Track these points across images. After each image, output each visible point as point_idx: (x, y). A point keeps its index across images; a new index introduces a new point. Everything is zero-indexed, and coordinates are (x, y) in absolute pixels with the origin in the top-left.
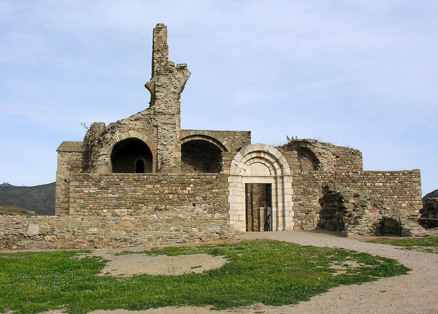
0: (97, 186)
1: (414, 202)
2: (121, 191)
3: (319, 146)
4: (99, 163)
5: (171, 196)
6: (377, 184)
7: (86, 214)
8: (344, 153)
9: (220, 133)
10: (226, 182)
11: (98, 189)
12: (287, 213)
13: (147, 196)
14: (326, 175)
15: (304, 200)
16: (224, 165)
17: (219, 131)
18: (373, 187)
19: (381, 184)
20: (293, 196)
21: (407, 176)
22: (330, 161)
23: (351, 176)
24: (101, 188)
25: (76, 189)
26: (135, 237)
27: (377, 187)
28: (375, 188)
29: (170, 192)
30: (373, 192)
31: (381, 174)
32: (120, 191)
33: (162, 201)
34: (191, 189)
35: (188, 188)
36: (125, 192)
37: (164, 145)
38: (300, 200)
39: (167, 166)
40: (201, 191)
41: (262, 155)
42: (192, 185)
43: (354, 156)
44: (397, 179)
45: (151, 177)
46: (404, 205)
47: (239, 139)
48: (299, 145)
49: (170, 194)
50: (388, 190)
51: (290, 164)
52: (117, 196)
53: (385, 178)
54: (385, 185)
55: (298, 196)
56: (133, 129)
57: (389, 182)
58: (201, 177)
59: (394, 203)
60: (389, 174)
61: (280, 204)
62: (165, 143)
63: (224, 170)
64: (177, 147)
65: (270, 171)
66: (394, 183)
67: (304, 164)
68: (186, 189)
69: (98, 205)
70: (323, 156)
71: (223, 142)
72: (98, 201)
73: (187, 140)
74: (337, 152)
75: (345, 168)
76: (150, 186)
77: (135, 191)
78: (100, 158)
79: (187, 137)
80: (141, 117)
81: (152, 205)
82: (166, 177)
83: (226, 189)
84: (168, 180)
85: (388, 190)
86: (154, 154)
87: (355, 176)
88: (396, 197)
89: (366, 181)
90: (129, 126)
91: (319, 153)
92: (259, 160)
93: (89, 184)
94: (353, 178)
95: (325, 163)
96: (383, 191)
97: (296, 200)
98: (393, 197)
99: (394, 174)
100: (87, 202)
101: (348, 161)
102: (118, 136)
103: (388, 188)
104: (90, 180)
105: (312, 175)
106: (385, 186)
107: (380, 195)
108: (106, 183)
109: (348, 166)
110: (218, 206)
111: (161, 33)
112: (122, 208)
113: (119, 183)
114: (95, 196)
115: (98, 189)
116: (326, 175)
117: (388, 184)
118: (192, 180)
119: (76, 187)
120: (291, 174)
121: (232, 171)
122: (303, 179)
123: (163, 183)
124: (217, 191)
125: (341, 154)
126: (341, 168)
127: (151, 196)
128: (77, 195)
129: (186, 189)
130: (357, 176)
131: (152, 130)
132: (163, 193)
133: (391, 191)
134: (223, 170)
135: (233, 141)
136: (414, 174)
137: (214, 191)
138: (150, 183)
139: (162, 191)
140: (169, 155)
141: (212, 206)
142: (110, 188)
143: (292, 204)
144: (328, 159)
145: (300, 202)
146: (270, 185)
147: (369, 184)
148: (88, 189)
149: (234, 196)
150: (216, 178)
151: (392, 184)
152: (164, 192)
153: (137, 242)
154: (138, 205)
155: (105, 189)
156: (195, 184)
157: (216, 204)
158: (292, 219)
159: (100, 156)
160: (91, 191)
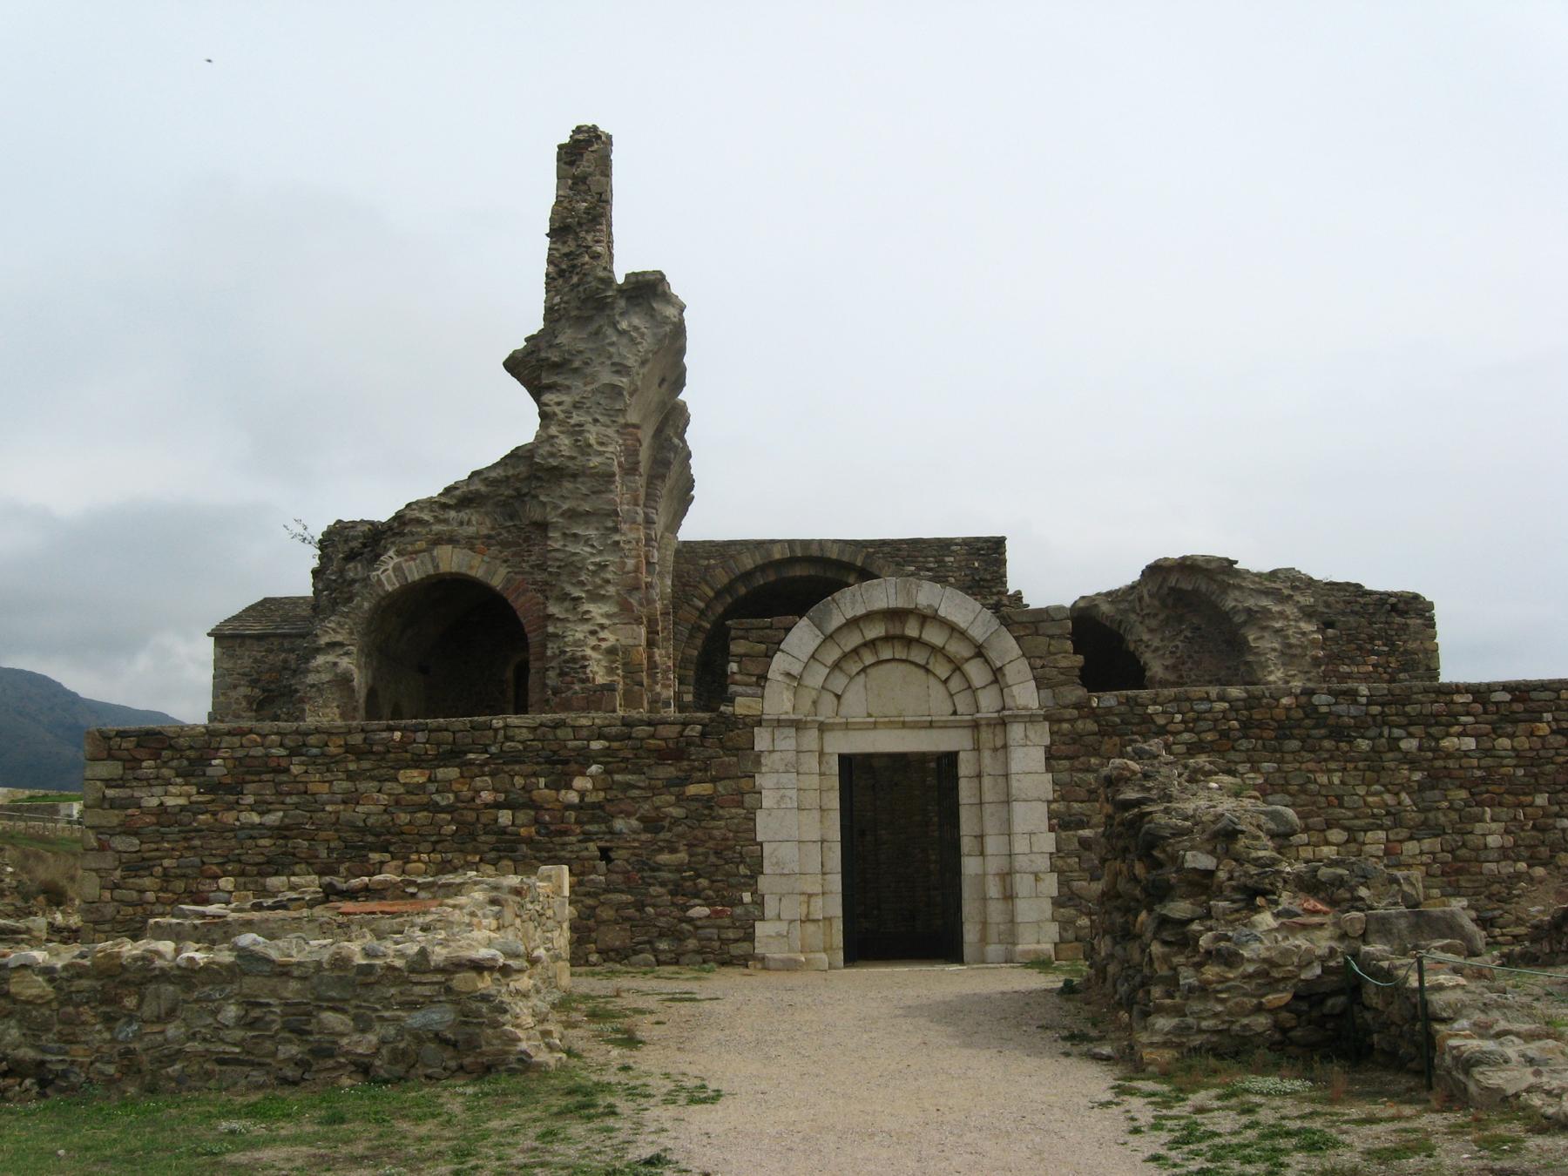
0: (194, 780)
2: (295, 799)
4: (311, 678)
5: (505, 817)
7: (150, 896)
8: (1357, 608)
10: (745, 750)
11: (199, 793)
12: (1023, 884)
13: (404, 818)
14: (1203, 707)
16: (738, 677)
18: (1430, 754)
19: (1470, 743)
20: (1054, 806)
23: (1324, 709)
24: (213, 788)
25: (110, 793)
26: (60, 1052)
27: (1449, 756)
28: (1439, 763)
29: (502, 797)
30: (1435, 779)
31: (1468, 698)
32: (288, 800)
34: (589, 786)
35: (579, 782)
36: (312, 804)
38: (1081, 825)
39: (577, 687)
40: (636, 793)
41: (912, 630)
42: (594, 769)
43: (1398, 620)
44: (1548, 716)
45: (421, 737)
47: (960, 568)
48: (1165, 579)
49: (498, 806)
50: (1503, 770)
51: (1039, 662)
52: (273, 818)
53: (1485, 712)
54: (1489, 745)
55: (1075, 805)
56: (452, 540)
57: (1510, 730)
59: (1534, 827)
60: (1508, 697)
61: (993, 844)
63: (738, 699)
65: (951, 695)
66: (1532, 734)
67: (1190, 657)
68: (569, 787)
69: (197, 860)
72: (197, 842)
73: (760, 581)
74: (1327, 605)
75: (1363, 669)
76: (415, 776)
77: (352, 799)
78: (320, 660)
79: (762, 568)
80: (483, 489)
81: (424, 857)
83: (744, 784)
84: (493, 749)
85: (1503, 770)
86: (533, 638)
87: (1342, 709)
88: (1541, 799)
89: (1397, 732)
92: (900, 653)
93: (165, 772)
94: (1332, 721)
96: (1478, 773)
97: (1065, 826)
98: (1529, 799)
99: (1534, 695)
100: (153, 846)
101: (1371, 639)
102: (390, 572)
103: (1506, 761)
104: (166, 754)
106: (1488, 752)
107: (1463, 794)
108: (230, 763)
110: (713, 859)
111: (586, 165)
112: (297, 869)
113: (284, 763)
114: (186, 820)
115: (199, 793)
116: (1203, 707)
117: (1505, 742)
118: (596, 745)
119: (109, 783)
120: (1041, 707)
121: (778, 701)
122: (1095, 728)
123: (471, 763)
124: (703, 789)
125: (1343, 613)
126: (1344, 669)
130: (1353, 710)
131: (527, 539)
132: (472, 805)
133: (1520, 772)
134: (731, 701)
137: (692, 790)
138: (417, 762)
140: (593, 641)
141: (683, 856)
142: (250, 787)
143: (1048, 842)
146: (951, 759)
147: (1409, 745)
148: (158, 790)
149: (781, 813)
150: (703, 735)
151: (1523, 742)
152: (478, 801)
153: (73, 1079)
155: (230, 789)
157: (700, 850)
158: (1047, 907)
159: (318, 650)
160: (170, 802)
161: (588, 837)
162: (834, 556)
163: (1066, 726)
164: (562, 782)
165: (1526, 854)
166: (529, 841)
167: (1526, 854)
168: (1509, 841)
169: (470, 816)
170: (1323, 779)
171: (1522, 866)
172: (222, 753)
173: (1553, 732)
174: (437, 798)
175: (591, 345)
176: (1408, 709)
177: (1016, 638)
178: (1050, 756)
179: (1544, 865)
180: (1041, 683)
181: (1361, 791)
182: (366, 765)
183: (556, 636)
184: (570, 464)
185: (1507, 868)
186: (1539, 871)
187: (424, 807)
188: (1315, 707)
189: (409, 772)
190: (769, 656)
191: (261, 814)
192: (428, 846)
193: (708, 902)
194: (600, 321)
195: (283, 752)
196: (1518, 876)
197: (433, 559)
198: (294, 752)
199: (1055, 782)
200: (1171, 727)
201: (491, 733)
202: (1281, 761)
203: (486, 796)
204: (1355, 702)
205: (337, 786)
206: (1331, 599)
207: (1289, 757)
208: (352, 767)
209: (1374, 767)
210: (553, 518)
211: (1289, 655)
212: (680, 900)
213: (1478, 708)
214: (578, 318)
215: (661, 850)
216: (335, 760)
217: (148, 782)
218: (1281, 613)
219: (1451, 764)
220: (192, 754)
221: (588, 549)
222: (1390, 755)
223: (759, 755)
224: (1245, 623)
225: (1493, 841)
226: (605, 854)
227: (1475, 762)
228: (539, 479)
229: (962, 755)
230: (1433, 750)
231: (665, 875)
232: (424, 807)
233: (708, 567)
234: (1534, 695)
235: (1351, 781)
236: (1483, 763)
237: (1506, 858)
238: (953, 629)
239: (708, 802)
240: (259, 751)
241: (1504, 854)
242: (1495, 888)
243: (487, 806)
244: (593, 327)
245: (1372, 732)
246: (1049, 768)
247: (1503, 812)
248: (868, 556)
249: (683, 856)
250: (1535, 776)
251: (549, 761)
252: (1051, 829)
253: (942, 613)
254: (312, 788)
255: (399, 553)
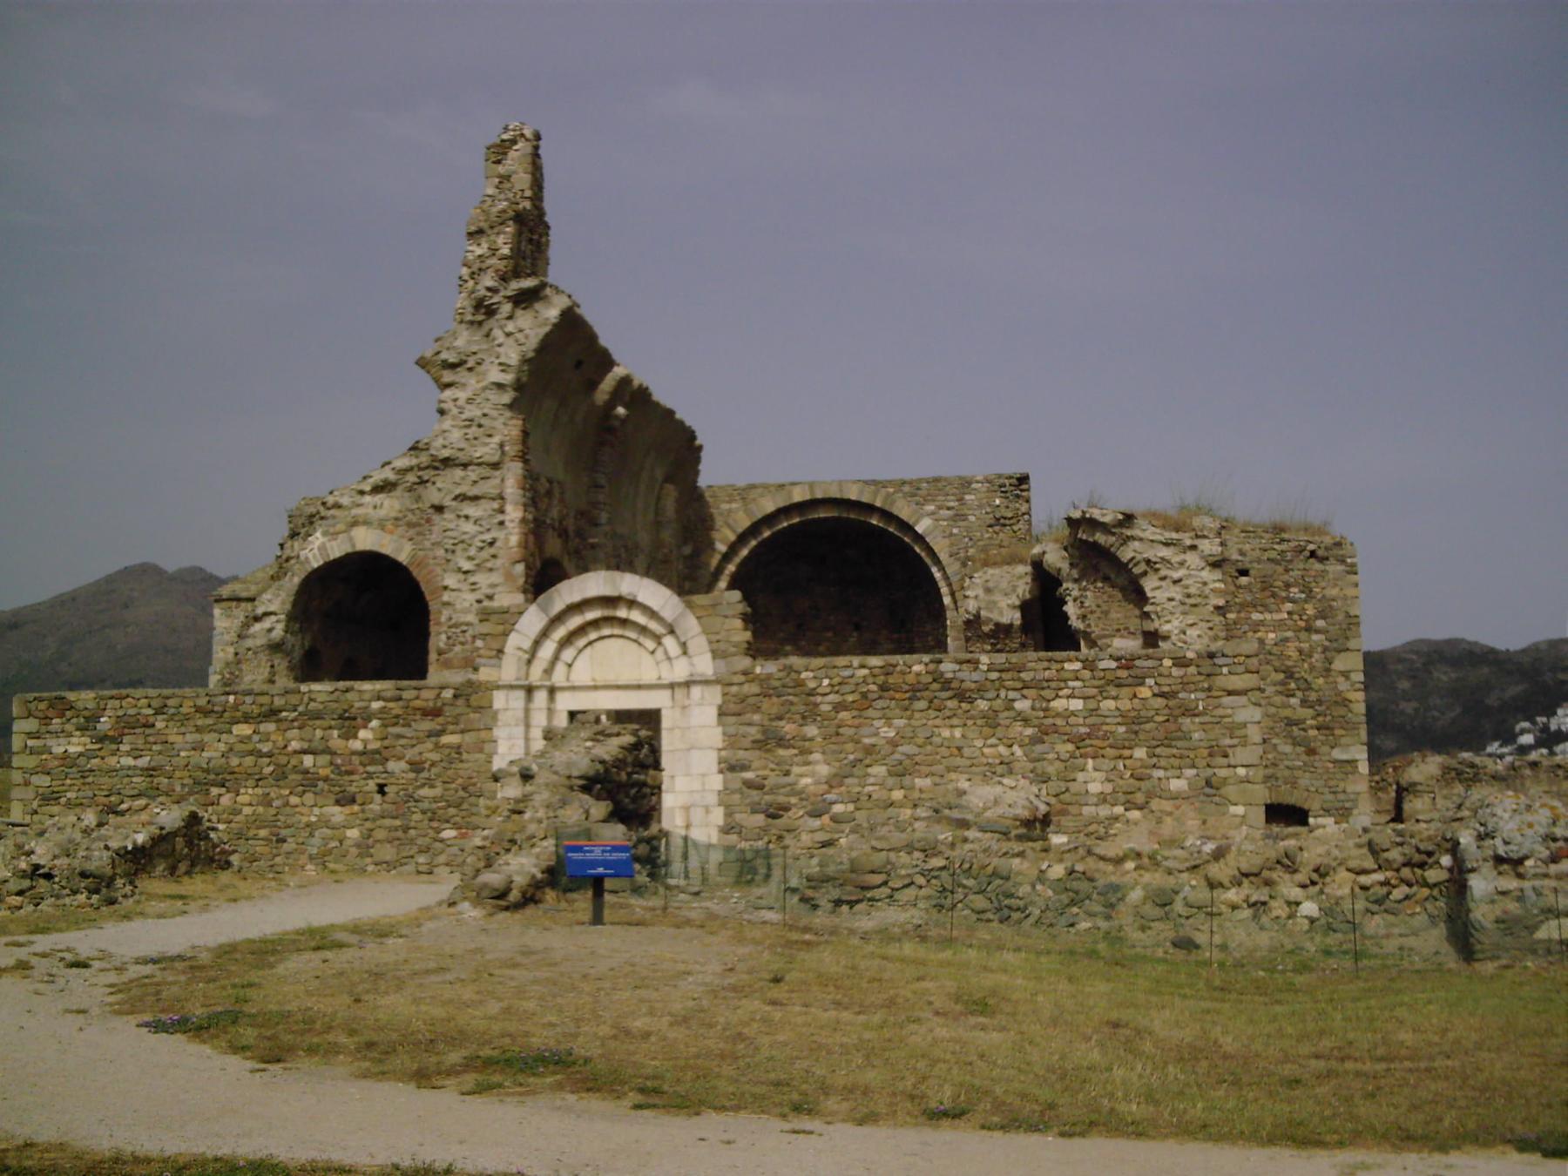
1: (1223, 773)
3: (1147, 535)
5: (308, 761)
6: (1059, 704)
8: (1273, 554)
9: (906, 488)
10: (485, 708)
14: (847, 673)
15: (765, 768)
17: (904, 483)
18: (1041, 714)
19: (1076, 704)
20: (723, 753)
21: (1192, 670)
22: (1192, 590)
23: (950, 675)
24: (102, 739)
25: (30, 743)
27: (1058, 715)
28: (1049, 721)
30: (1044, 733)
32: (154, 747)
33: (280, 776)
37: (466, 572)
38: (744, 768)
40: (403, 742)
41: (622, 613)
42: (375, 723)
43: (1318, 566)
45: (249, 699)
46: (1177, 785)
47: (980, 507)
49: (305, 752)
52: (143, 762)
56: (367, 523)
57: (1113, 693)
58: (406, 695)
60: (1113, 664)
62: (467, 566)
64: (509, 576)
66: (1135, 696)
68: (355, 737)
70: (1163, 573)
71: (917, 522)
72: (90, 780)
74: (1242, 553)
75: (1277, 616)
76: (243, 730)
77: (199, 747)
82: (294, 699)
83: (483, 734)
85: (1105, 728)
88: (1140, 753)
89: (1012, 695)
90: (355, 511)
91: (1148, 562)
92: (617, 631)
93: (69, 727)
94: (955, 685)
95: (1171, 600)
97: (732, 768)
101: (1288, 586)
105: (793, 675)
106: (1094, 711)
107: (1070, 747)
109: (1289, 606)
110: (461, 793)
113: (151, 720)
116: (847, 673)
117: (1111, 704)
118: (376, 705)
119: (31, 735)
125: (1259, 561)
126: (1256, 616)
127: (249, 761)
128: (31, 762)
129: (355, 737)
130: (976, 676)
131: (428, 521)
133: (1122, 729)
135: (959, 517)
136: (1229, 661)
137: (445, 739)
138: (246, 719)
139: (281, 744)
144: (1187, 587)
145: (749, 775)
148: (61, 740)
150: (455, 696)
151: (1125, 704)
154: (207, 792)
156: (389, 720)
160: (72, 749)
161: (370, 776)
162: (853, 498)
163: (734, 689)
164: (350, 734)
165: (1122, 798)
166: (326, 779)
167: (1122, 798)
168: (1108, 788)
169: (283, 760)
170: (946, 733)
171: (1119, 810)
172: (108, 713)
173: (1155, 695)
174: (259, 746)
175: (485, 346)
176: (1023, 675)
177: (698, 618)
178: (722, 713)
179: (1140, 808)
180: (715, 655)
181: (979, 743)
182: (209, 721)
183: (448, 604)
184: (460, 454)
185: (1104, 811)
186: (1135, 814)
187: (251, 753)
188: (942, 674)
189: (241, 726)
190: (506, 634)
191: (135, 758)
192: (251, 783)
193: (457, 827)
194: (492, 323)
195: (151, 712)
196: (1116, 818)
197: (351, 539)
198: (159, 711)
199: (724, 734)
200: (820, 690)
201: (298, 697)
202: (909, 718)
203: (295, 745)
204: (976, 669)
205: (189, 737)
206: (1247, 547)
207: (917, 715)
208: (200, 722)
209: (991, 721)
210: (447, 502)
211: (1190, 604)
212: (435, 824)
213: (1087, 674)
214: (472, 323)
215: (423, 785)
216: (187, 717)
217: (56, 734)
218: (1182, 564)
219: (1059, 722)
220: (86, 713)
221: (477, 528)
222: (1006, 714)
223: (496, 713)
224: (1145, 573)
225: (1094, 788)
226: (381, 789)
227: (1081, 721)
228: (436, 468)
229: (664, 712)
230: (1046, 710)
231: (425, 805)
232: (251, 753)
233: (730, 511)
234: (1137, 663)
235: (970, 735)
236: (1088, 721)
237: (1105, 801)
238: (652, 614)
239: (458, 749)
240: (132, 712)
241: (1103, 799)
242: (1092, 828)
243: (296, 752)
244: (486, 327)
245: (991, 694)
246: (720, 723)
247: (1106, 764)
248: (888, 495)
249: (438, 791)
250: (1136, 733)
251: (341, 717)
252: (721, 772)
253: (640, 599)
254: (171, 739)
255: (325, 534)
